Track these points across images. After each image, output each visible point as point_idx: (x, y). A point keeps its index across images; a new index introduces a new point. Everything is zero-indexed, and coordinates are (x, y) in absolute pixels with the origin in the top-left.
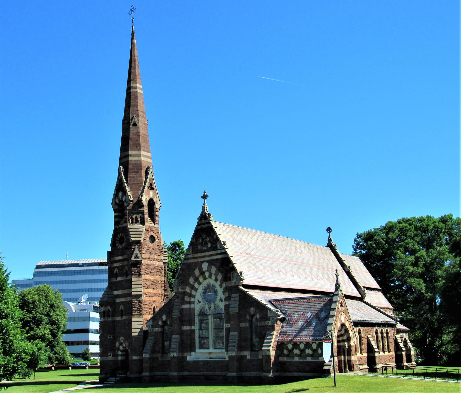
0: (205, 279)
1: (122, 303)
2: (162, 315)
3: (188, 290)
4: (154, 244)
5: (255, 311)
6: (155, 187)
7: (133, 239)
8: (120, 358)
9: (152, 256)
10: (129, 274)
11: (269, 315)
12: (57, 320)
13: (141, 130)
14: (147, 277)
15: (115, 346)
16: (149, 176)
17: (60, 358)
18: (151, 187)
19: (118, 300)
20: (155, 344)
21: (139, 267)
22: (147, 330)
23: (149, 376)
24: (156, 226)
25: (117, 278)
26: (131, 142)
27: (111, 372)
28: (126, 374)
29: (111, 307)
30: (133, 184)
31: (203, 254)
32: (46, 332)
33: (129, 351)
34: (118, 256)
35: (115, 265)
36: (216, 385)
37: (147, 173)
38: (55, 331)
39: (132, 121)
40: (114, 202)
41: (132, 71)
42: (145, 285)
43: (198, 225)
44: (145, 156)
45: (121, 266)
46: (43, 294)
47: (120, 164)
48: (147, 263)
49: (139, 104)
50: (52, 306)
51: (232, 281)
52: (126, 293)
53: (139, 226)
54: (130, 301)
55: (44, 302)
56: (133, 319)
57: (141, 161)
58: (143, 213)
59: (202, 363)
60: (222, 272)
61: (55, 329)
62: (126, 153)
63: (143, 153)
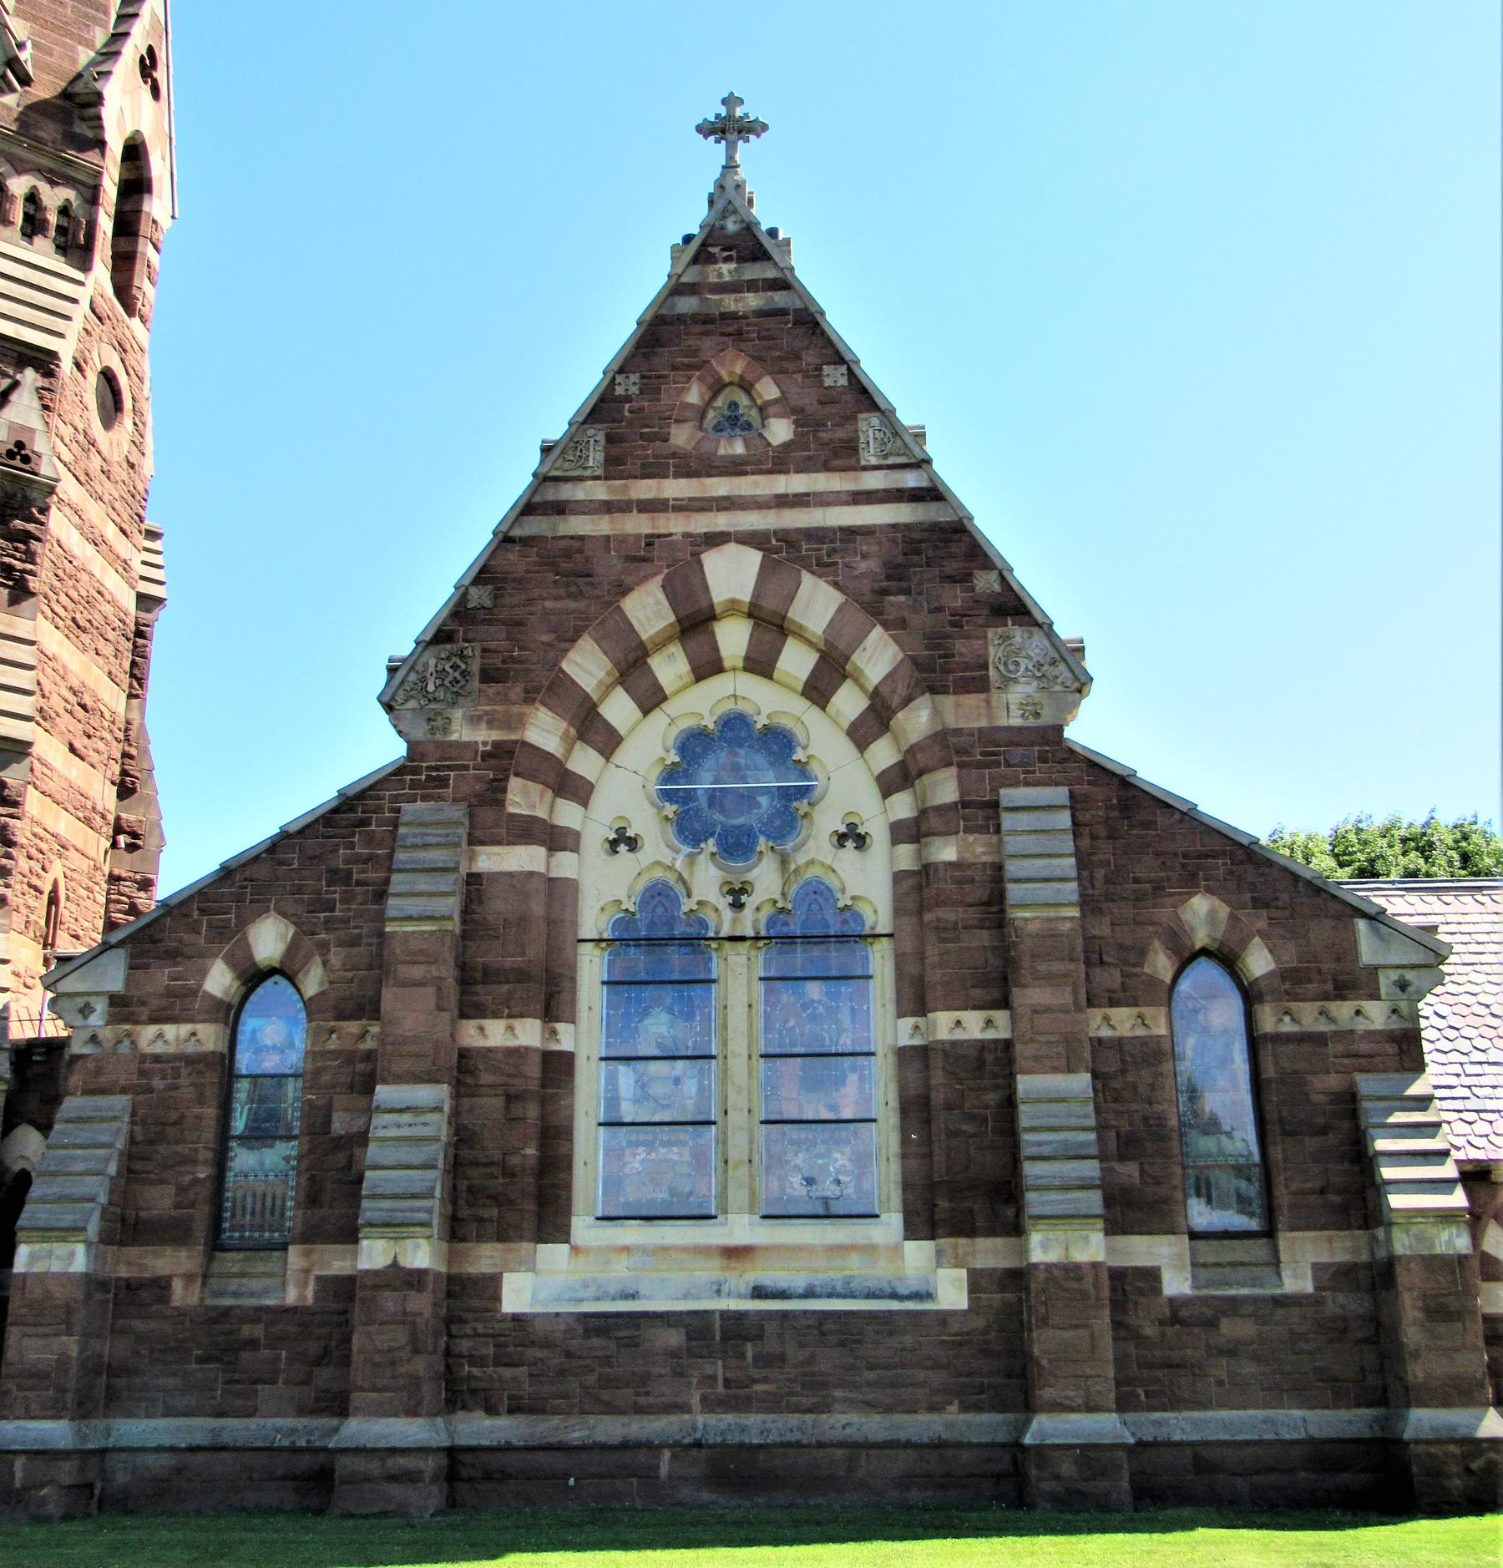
0: (707, 666)
2: (243, 923)
3: (544, 730)
4: (110, 434)
5: (1233, 918)
11: (1368, 948)
14: (52, 639)
21: (27, 537)
22: (53, 1047)
31: (720, 487)
36: (976, 1536)
43: (676, 288)
51: (996, 697)
58: (93, 197)
59: (674, 1338)
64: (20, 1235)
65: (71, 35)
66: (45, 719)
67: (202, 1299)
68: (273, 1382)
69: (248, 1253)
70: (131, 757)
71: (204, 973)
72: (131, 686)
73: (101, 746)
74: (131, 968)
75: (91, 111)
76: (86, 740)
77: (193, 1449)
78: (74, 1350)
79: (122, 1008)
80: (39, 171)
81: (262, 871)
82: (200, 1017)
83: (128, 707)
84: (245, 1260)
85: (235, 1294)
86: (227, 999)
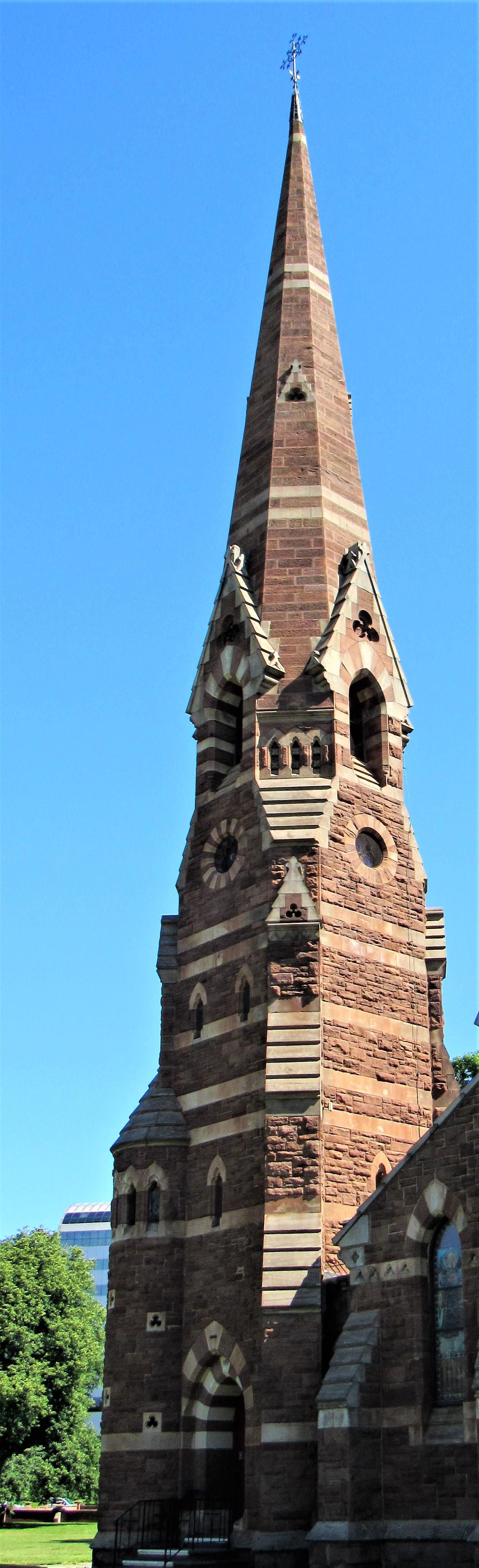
1: (221, 1147)
2: (423, 1188)
4: (380, 868)
6: (382, 632)
7: (278, 835)
8: (201, 1440)
9: (371, 923)
10: (250, 999)
12: (71, 1346)
13: (320, 415)
14: (347, 1016)
15: (178, 1376)
16: (358, 580)
17: (79, 1479)
18: (364, 625)
19: (202, 1136)
20: (382, 1355)
21: (307, 961)
22: (344, 1280)
23: (349, 1544)
24: (388, 790)
25: (199, 1028)
26: (279, 457)
27: (135, 1511)
28: (229, 1533)
29: (166, 1168)
30: (285, 608)
32: (28, 1384)
33: (249, 1401)
34: (210, 924)
35: (195, 969)
37: (346, 569)
38: (60, 1383)
39: (284, 382)
40: (198, 701)
41: (289, 224)
42: (335, 1053)
44: (334, 508)
45: (224, 967)
46: (32, 1257)
47: (231, 542)
48: (344, 949)
49: (313, 327)
50: (57, 1297)
52: (241, 1092)
53: (308, 778)
54: (257, 1131)
55: (31, 1284)
56: (271, 1222)
57: (319, 521)
58: (329, 727)
61: (61, 1378)
62: (257, 500)
63: (327, 493)
64: (319, 1406)
65: (304, 633)
66: (350, 1067)
67: (424, 1441)
68: (463, 1495)
69: (451, 1408)
70: (439, 1069)
71: (405, 1225)
72: (431, 1022)
73: (408, 1069)
74: (373, 1227)
75: (319, 677)
76: (393, 1069)
77: (424, 1541)
78: (348, 1477)
79: (373, 1254)
80: (296, 727)
81: (426, 1153)
82: (407, 1255)
83: (431, 1037)
84: (449, 1412)
85: (441, 1437)
86: (421, 1240)
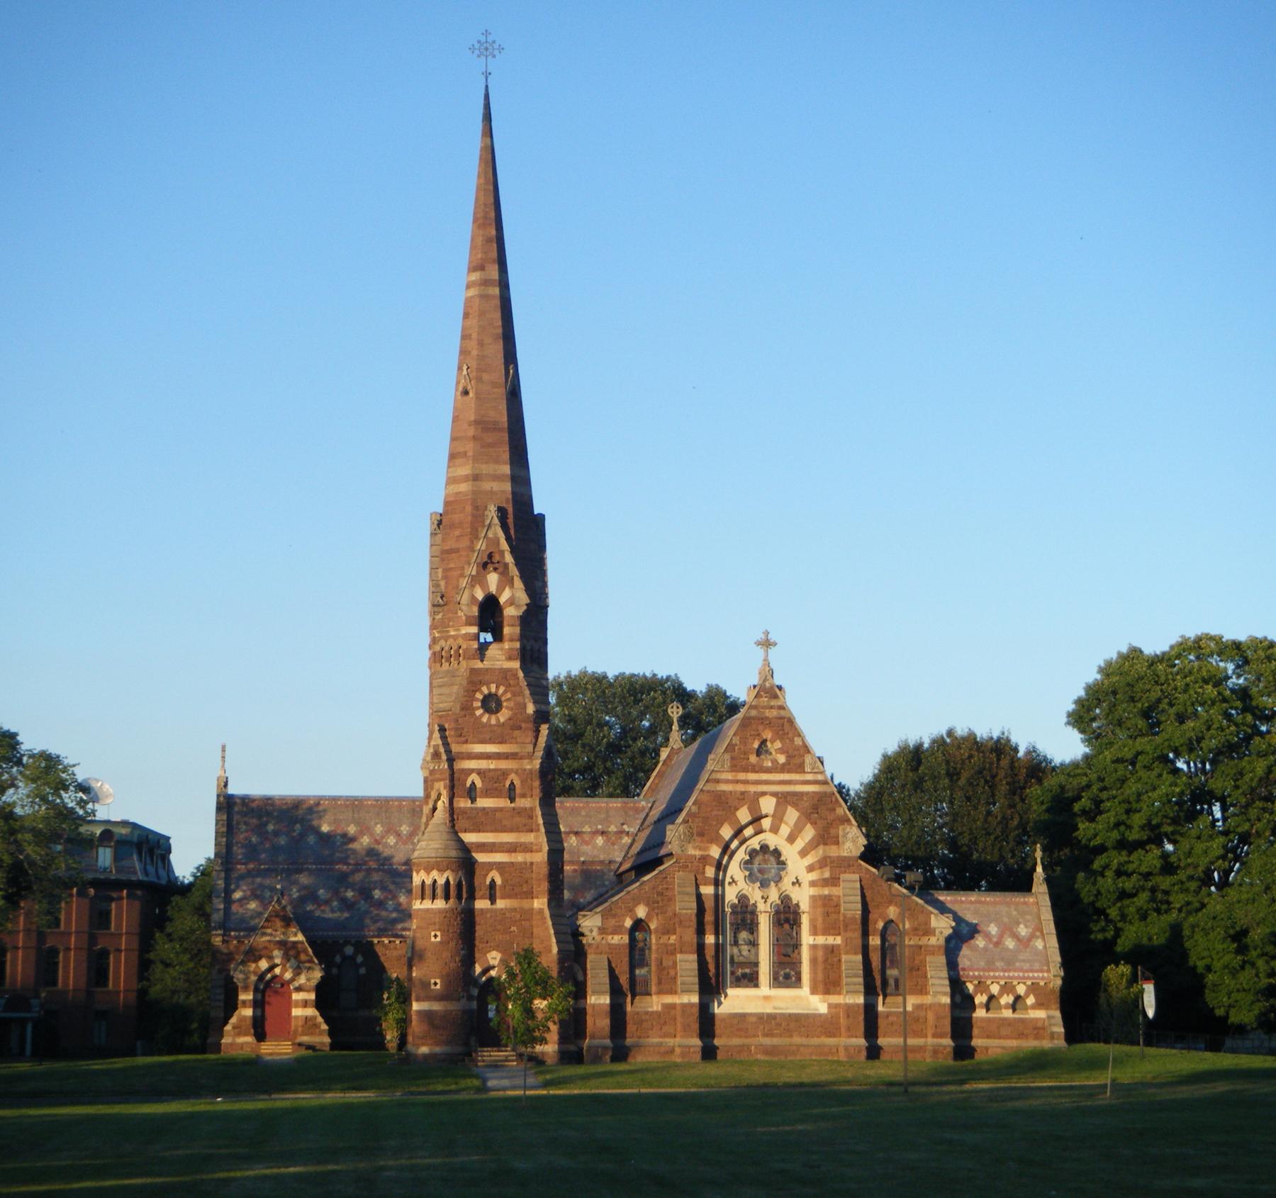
31: (765, 777)
59: (754, 1019)
60: (814, 824)
